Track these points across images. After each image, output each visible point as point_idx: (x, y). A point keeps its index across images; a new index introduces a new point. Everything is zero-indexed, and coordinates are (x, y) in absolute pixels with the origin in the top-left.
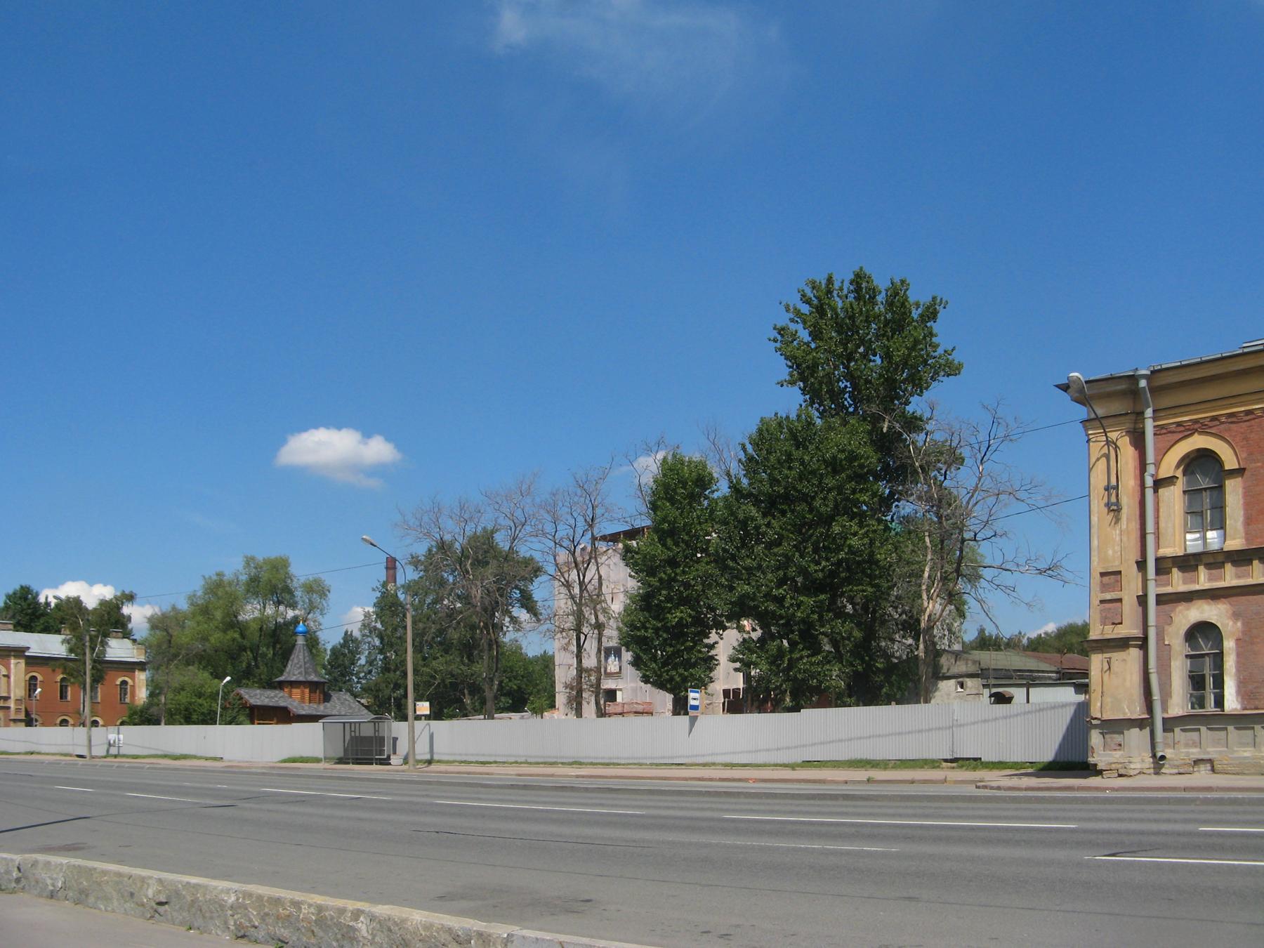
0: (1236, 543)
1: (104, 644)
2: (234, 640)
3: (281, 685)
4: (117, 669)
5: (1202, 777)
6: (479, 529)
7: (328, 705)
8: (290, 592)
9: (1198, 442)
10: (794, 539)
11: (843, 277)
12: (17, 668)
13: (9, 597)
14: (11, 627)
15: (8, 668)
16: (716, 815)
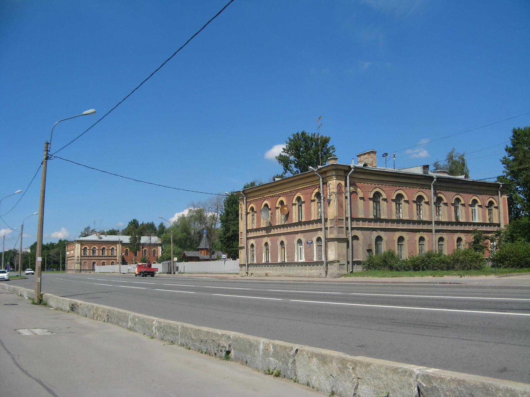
0: (255, 228)
1: (140, 238)
3: (198, 250)
4: (111, 244)
5: (252, 277)
6: (224, 211)
12: (119, 246)
13: (129, 223)
14: (236, 242)
15: (117, 247)
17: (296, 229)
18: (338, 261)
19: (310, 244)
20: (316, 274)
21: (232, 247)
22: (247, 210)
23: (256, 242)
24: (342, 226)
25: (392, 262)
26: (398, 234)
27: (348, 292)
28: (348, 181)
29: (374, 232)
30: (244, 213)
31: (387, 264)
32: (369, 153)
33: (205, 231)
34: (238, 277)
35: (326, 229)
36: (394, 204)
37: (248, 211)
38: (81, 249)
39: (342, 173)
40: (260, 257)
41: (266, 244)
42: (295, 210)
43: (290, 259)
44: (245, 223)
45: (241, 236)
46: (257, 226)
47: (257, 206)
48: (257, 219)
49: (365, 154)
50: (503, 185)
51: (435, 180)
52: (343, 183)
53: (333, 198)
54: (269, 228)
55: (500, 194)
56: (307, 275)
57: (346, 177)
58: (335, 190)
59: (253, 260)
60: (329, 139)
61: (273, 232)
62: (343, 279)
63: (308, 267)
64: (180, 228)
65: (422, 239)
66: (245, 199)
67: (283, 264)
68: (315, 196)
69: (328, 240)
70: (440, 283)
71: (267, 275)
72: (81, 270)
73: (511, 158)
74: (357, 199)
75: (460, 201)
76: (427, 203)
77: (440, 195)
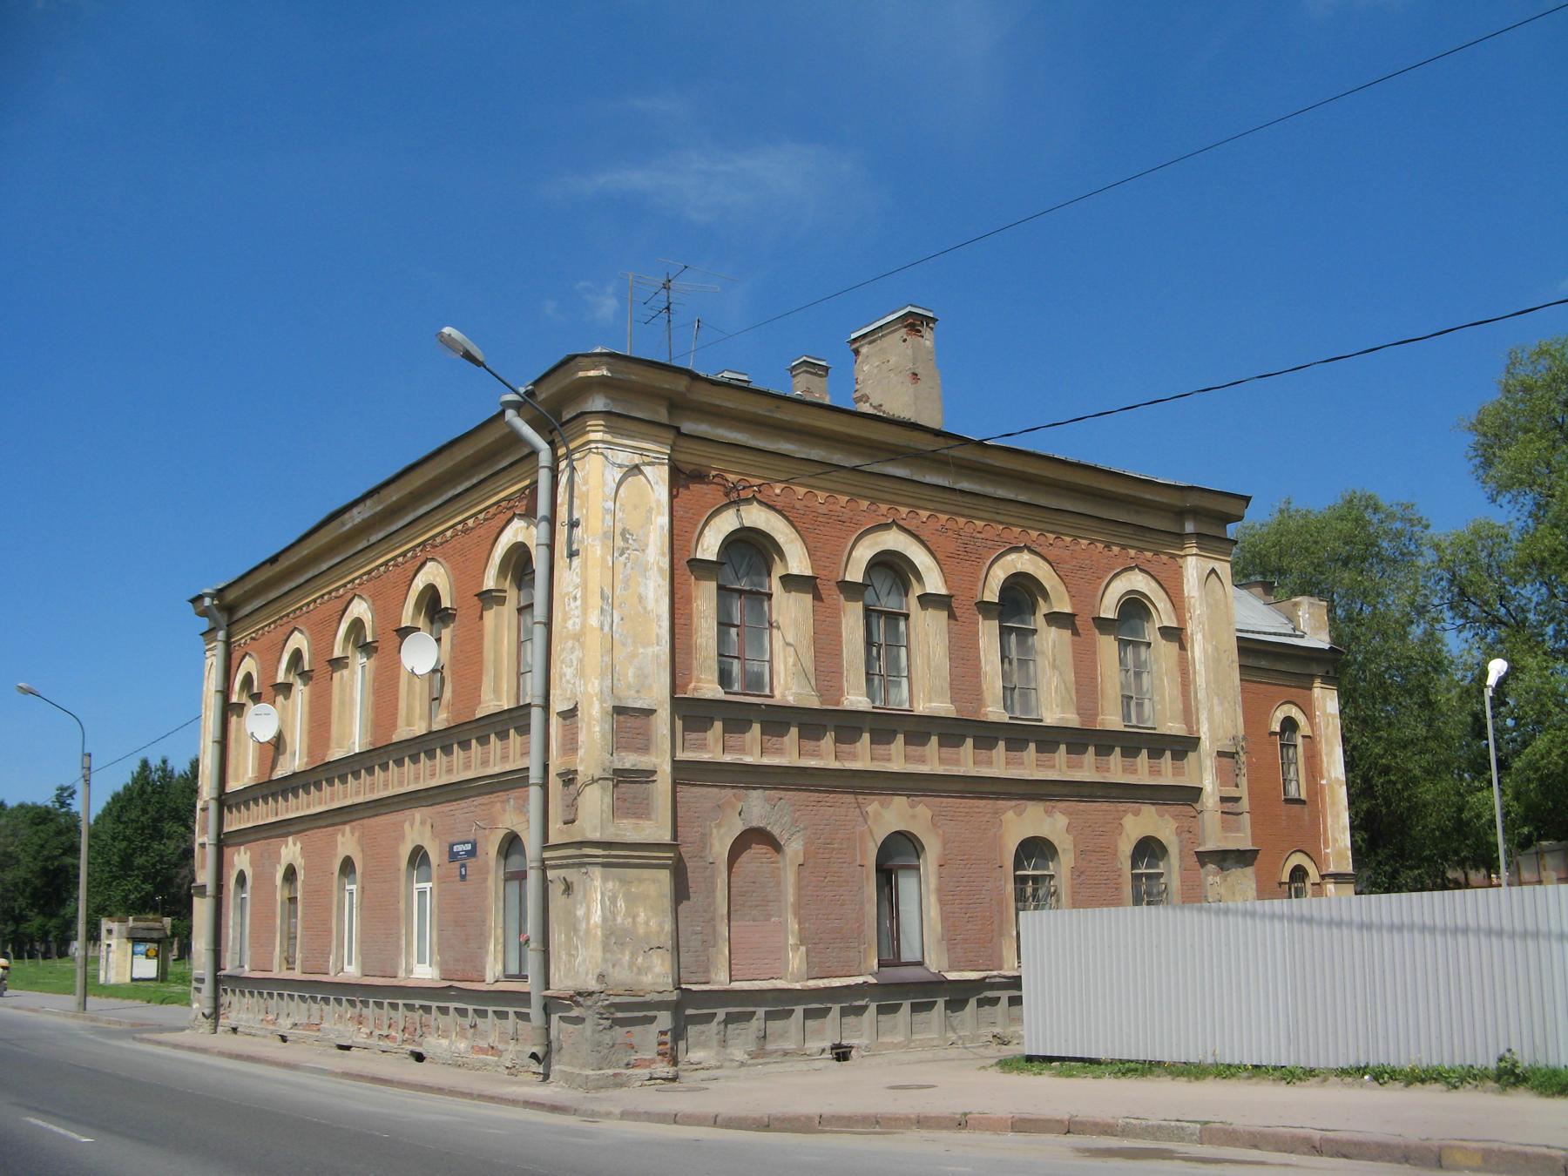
36: (988, 633)
38: (685, 567)
72: (689, 1008)
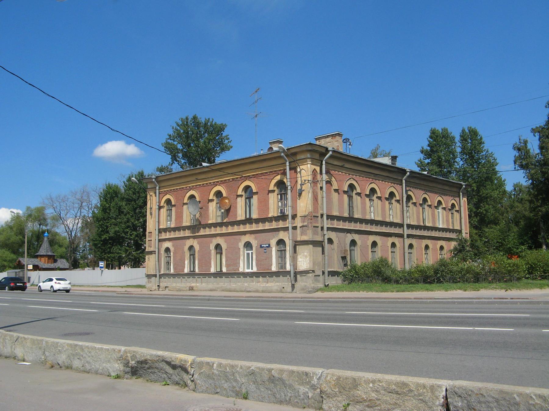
0: (173, 226)
2: (20, 239)
3: (37, 257)
5: (167, 292)
7: (55, 264)
8: (45, 219)
9: (247, 183)
10: (132, 213)
11: (190, 117)
16: (87, 302)
17: (242, 228)
18: (313, 271)
19: (265, 248)
20: (275, 288)
21: (110, 252)
22: (160, 202)
23: (173, 246)
24: (316, 225)
25: (388, 273)
26: (372, 238)
27: (186, 305)
28: (324, 166)
29: (349, 234)
30: (155, 207)
31: (379, 274)
32: (333, 136)
33: (46, 234)
34: (144, 291)
35: (295, 228)
37: (162, 204)
39: (317, 156)
40: (180, 264)
41: (191, 248)
42: (241, 202)
43: (231, 268)
44: (156, 219)
45: (150, 236)
46: (176, 223)
47: (177, 199)
48: (176, 215)
49: (328, 136)
50: (465, 185)
51: (408, 173)
52: (318, 169)
53: (307, 187)
54: (196, 227)
55: (461, 196)
56: (261, 289)
57: (322, 162)
58: (310, 178)
59: (169, 269)
60: (226, 126)
61: (202, 232)
62: (319, 294)
63: (261, 279)
64: (15, 229)
65: (374, 244)
66: (157, 188)
67: (219, 274)
68: (275, 185)
69: (296, 244)
70: (495, 298)
71: (191, 289)
73: (427, 161)
74: (331, 191)
75: (427, 201)
76: (398, 201)
77: (410, 193)
